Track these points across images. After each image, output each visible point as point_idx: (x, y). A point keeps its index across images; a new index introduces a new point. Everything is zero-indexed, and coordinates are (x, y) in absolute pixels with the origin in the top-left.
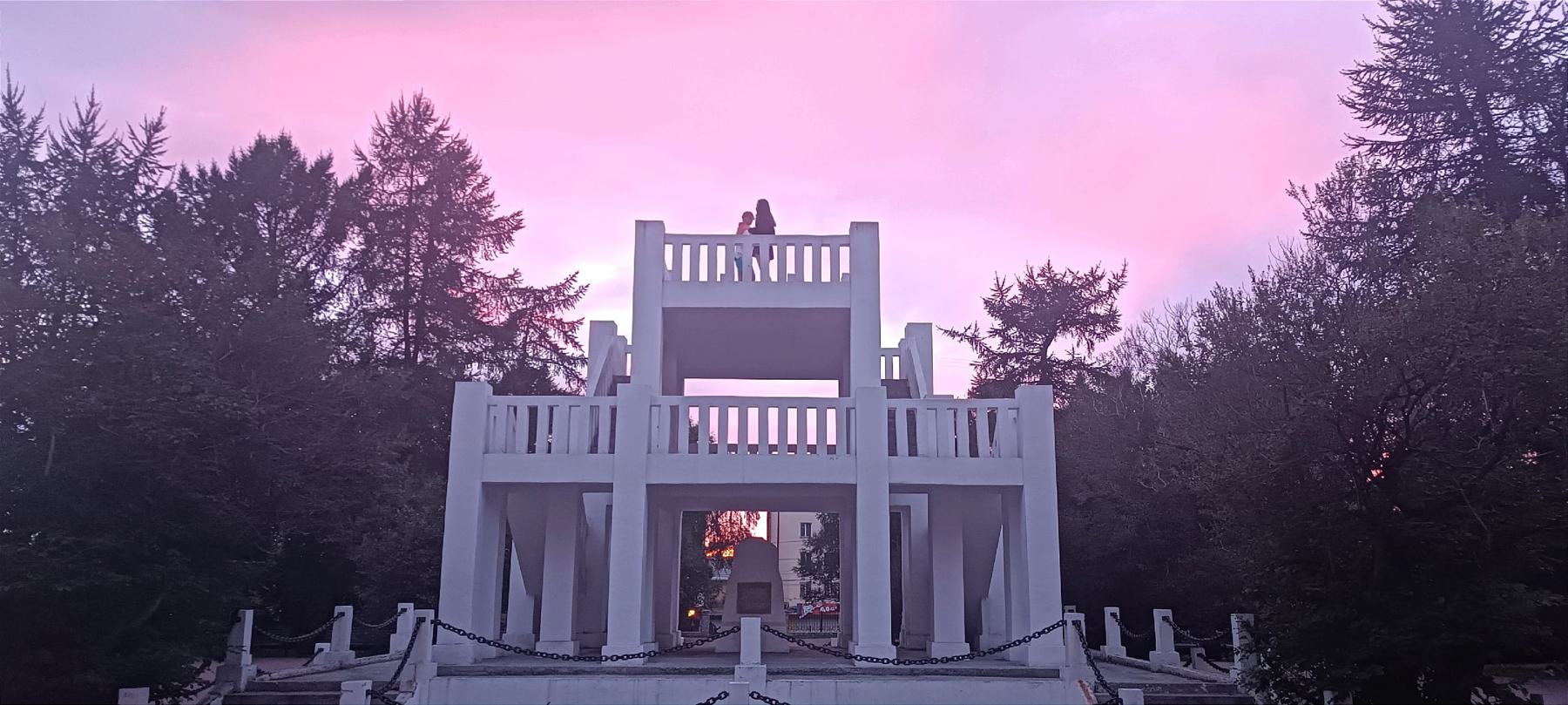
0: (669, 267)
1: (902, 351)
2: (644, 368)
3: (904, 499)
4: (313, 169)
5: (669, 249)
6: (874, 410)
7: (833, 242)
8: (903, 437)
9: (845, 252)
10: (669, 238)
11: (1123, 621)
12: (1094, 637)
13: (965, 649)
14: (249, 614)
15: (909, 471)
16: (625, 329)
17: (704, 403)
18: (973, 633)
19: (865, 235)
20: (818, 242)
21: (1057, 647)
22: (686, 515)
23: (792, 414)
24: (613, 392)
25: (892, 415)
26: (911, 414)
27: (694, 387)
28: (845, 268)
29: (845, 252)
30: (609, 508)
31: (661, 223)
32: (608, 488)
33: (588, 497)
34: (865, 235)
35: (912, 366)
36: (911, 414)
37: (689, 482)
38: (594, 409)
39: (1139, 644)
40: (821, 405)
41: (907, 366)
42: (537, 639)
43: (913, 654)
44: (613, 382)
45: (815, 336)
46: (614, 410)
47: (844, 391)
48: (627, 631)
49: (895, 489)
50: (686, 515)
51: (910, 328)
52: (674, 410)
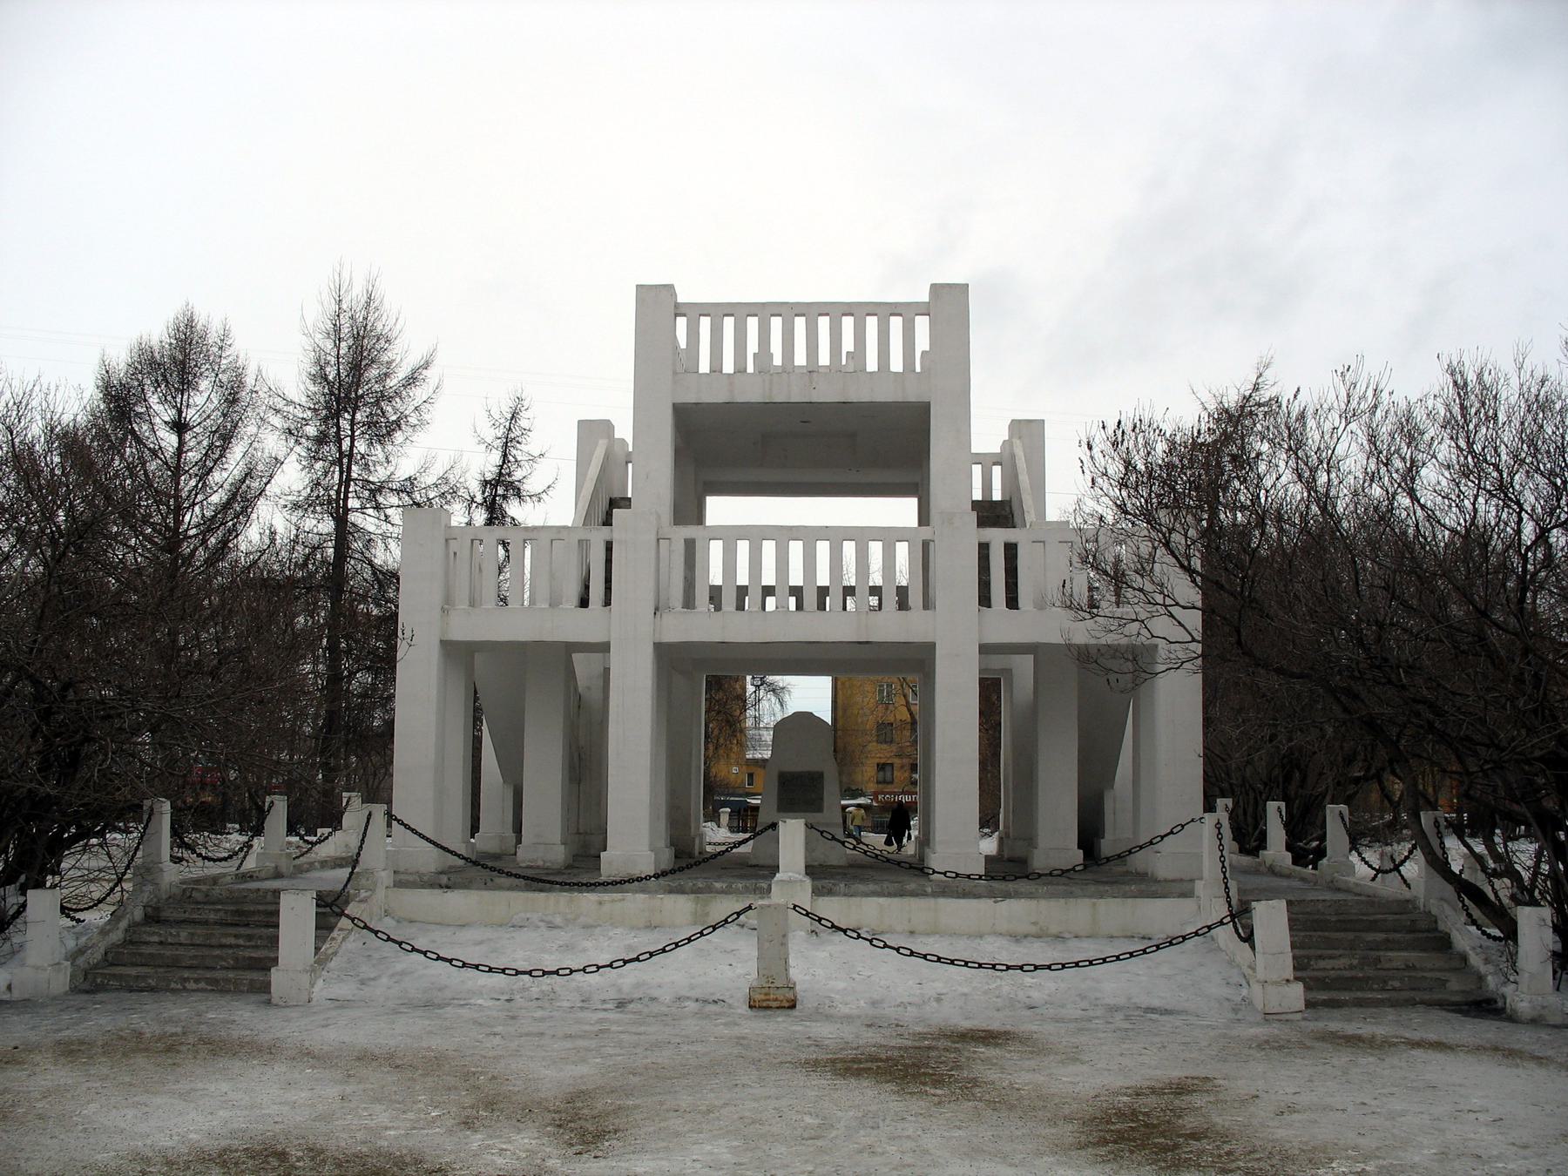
1: (1005, 459)
2: (651, 482)
3: (997, 662)
4: (834, 718)
5: (682, 323)
6: (961, 542)
7: (907, 311)
8: (999, 580)
9: (922, 324)
10: (679, 310)
12: (1248, 837)
14: (918, 369)
15: (1004, 626)
16: (624, 430)
17: (729, 535)
18: (1089, 836)
19: (949, 304)
20: (884, 311)
22: (708, 685)
23: (743, 547)
24: (608, 522)
25: (984, 548)
26: (1011, 550)
27: (722, 510)
28: (922, 342)
29: (922, 324)
30: (607, 671)
31: (672, 287)
32: (604, 648)
33: (576, 657)
34: (949, 304)
35: (1016, 476)
36: (1011, 550)
37: (962, 901)
38: (583, 545)
39: (1306, 848)
40: (889, 536)
41: (1011, 480)
42: (519, 841)
43: (1010, 870)
45: (874, 441)
46: (609, 547)
48: (632, 839)
49: (985, 649)
50: (708, 685)
51: (1017, 427)
52: (690, 545)
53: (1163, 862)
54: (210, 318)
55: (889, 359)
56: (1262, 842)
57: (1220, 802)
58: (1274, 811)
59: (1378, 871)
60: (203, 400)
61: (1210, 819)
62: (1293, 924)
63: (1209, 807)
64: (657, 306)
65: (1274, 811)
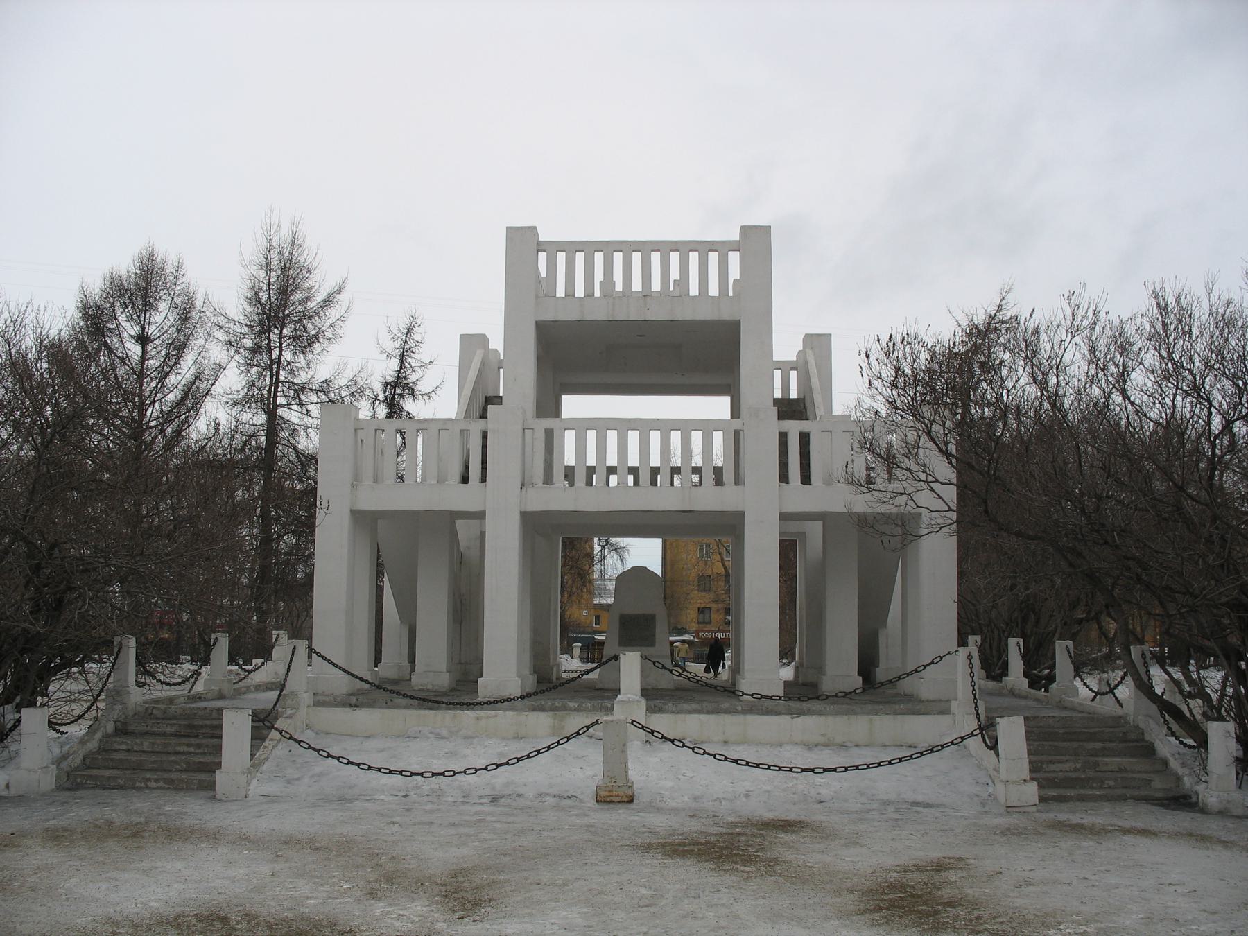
0: (543, 274)
1: (800, 366)
2: (518, 383)
3: (794, 527)
5: (542, 257)
6: (765, 432)
7: (722, 248)
8: (795, 461)
9: (734, 258)
10: (541, 247)
11: (1027, 657)
12: (994, 666)
13: (859, 681)
15: (799, 498)
16: (497, 343)
17: (580, 426)
18: (867, 665)
19: (755, 242)
20: (704, 247)
21: (957, 672)
22: (564, 546)
24: (484, 415)
25: (783, 437)
26: (805, 438)
27: (574, 406)
28: (734, 273)
29: (734, 258)
30: (483, 534)
32: (481, 515)
34: (755, 242)
35: (809, 379)
36: (805, 438)
39: (1040, 678)
40: (708, 427)
41: (804, 382)
42: (413, 669)
43: (804, 693)
44: (483, 402)
45: (695, 351)
46: (485, 436)
47: (735, 412)
48: (503, 667)
49: (784, 517)
50: (564, 546)
51: (810, 339)
52: (549, 434)
53: (926, 686)
54: (167, 253)
55: (708, 286)
56: (1004, 671)
57: (972, 639)
58: (1014, 645)
59: (1097, 693)
60: (161, 318)
61: (963, 652)
62: (1029, 735)
63: (962, 642)
64: (523, 243)
65: (1014, 645)
